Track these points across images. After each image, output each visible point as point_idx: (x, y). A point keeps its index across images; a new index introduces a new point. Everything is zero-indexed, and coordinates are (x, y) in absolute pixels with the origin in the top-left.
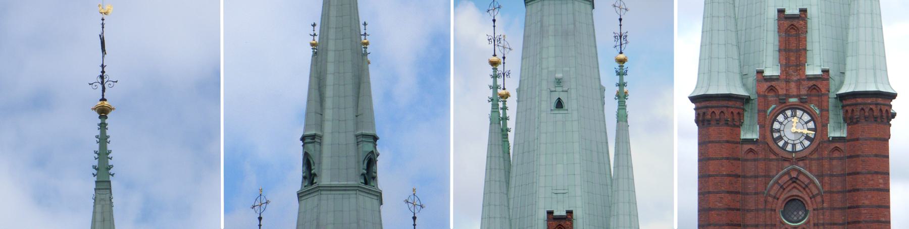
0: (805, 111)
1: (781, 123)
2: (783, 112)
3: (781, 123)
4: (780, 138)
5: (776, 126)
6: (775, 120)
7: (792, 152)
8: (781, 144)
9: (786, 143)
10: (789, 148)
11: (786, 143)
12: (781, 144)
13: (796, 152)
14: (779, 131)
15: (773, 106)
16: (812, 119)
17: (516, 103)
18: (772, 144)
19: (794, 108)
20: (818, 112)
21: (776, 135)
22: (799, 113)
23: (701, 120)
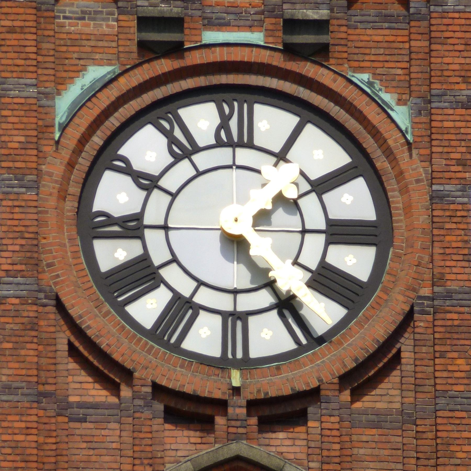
0: (309, 113)
1: (148, 183)
2: (162, 112)
3: (148, 183)
4: (142, 275)
5: (115, 195)
6: (107, 157)
7: (222, 364)
8: (148, 309)
9: (182, 309)
10: (204, 337)
11: (182, 309)
12: (148, 309)
13: (247, 364)
14: (132, 227)
15: (95, 73)
16: (362, 165)
17: (106, 72)
18: (59, 238)
19: (234, 85)
20: (401, 116)
21: (113, 254)
22: (271, 123)
23: (176, 42)
